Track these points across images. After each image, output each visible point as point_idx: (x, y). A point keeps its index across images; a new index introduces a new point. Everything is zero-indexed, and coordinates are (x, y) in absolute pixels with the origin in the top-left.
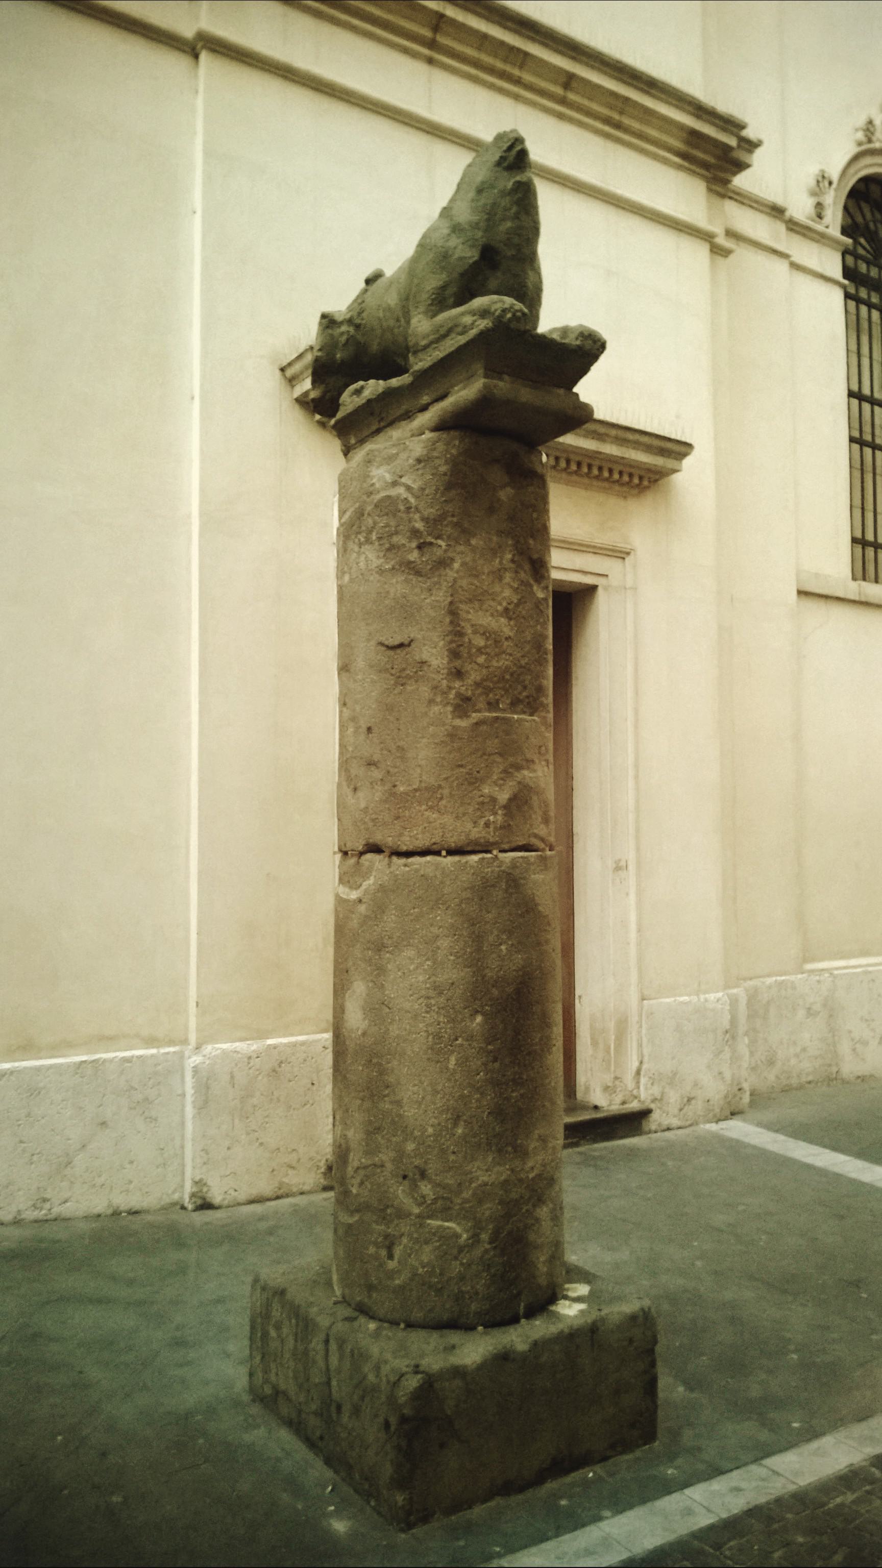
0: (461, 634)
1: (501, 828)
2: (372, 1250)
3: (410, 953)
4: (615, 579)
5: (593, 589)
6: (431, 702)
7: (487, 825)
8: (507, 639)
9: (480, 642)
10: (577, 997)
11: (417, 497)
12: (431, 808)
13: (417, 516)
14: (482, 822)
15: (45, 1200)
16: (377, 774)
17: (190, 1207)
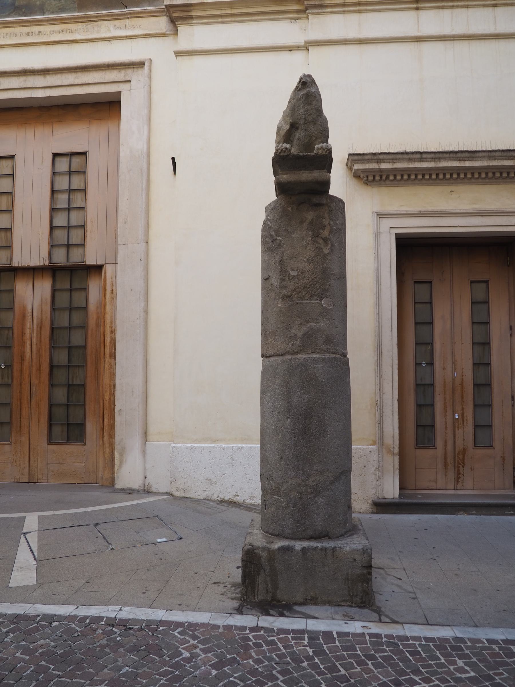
0: (286, 272)
1: (299, 346)
6: (275, 299)
7: (293, 345)
8: (308, 271)
9: (294, 273)
11: (271, 223)
12: (274, 339)
13: (272, 230)
14: (291, 344)
15: (254, 497)
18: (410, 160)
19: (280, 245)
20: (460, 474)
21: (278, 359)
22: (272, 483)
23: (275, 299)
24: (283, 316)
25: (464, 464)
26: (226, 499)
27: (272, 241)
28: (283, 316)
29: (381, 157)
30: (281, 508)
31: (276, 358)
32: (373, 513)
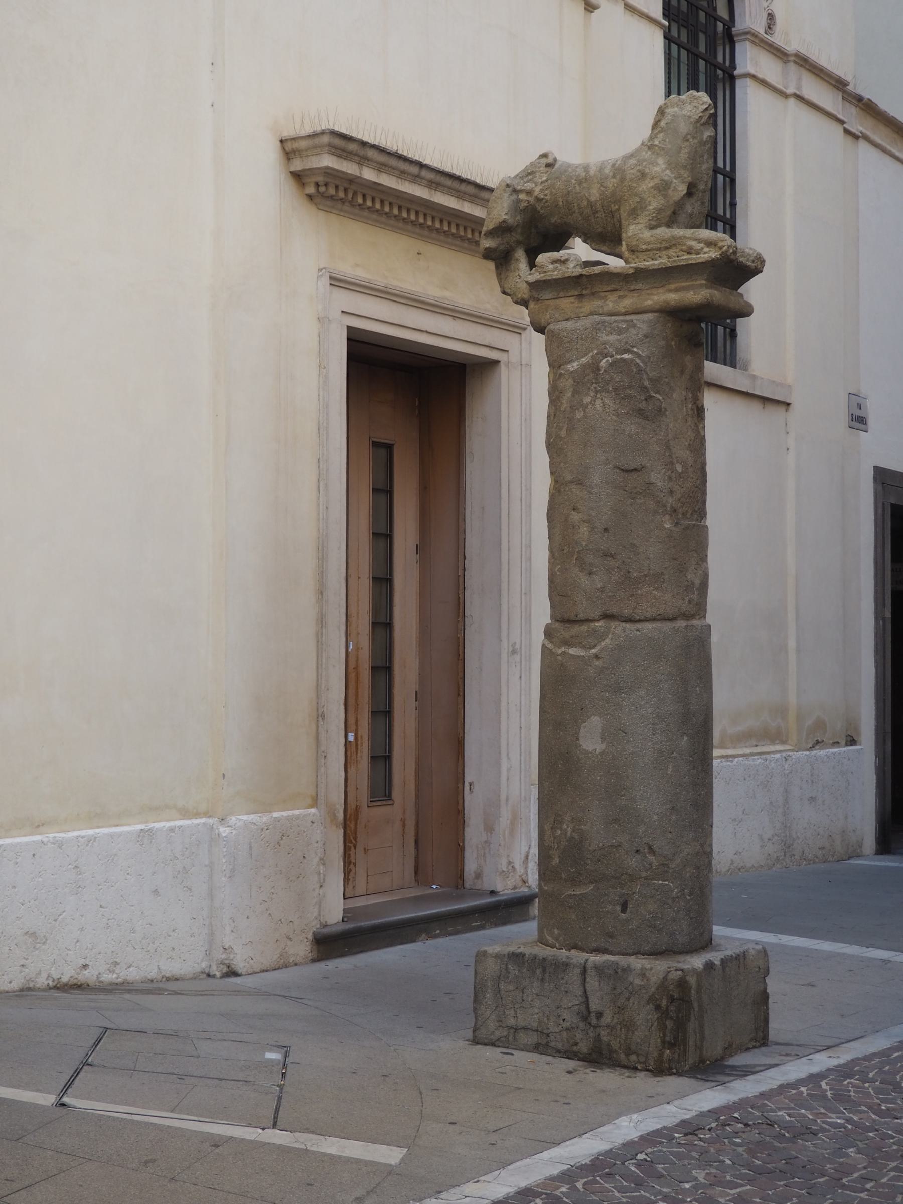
2: (609, 907)
3: (642, 693)
4: (514, 357)
5: (496, 363)
7: (690, 602)
10: (467, 784)
12: (656, 589)
14: (687, 600)
15: (116, 964)
16: (612, 563)
17: (218, 974)
18: (402, 174)
19: (660, 411)
20: (350, 863)
21: (666, 626)
22: (651, 858)
23: (655, 512)
24: (674, 547)
25: (355, 840)
26: (65, 979)
27: (646, 399)
28: (674, 547)
29: (371, 153)
30: (670, 902)
31: (658, 624)
32: (314, 961)
